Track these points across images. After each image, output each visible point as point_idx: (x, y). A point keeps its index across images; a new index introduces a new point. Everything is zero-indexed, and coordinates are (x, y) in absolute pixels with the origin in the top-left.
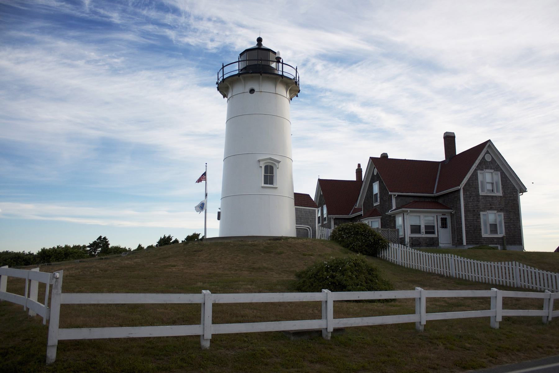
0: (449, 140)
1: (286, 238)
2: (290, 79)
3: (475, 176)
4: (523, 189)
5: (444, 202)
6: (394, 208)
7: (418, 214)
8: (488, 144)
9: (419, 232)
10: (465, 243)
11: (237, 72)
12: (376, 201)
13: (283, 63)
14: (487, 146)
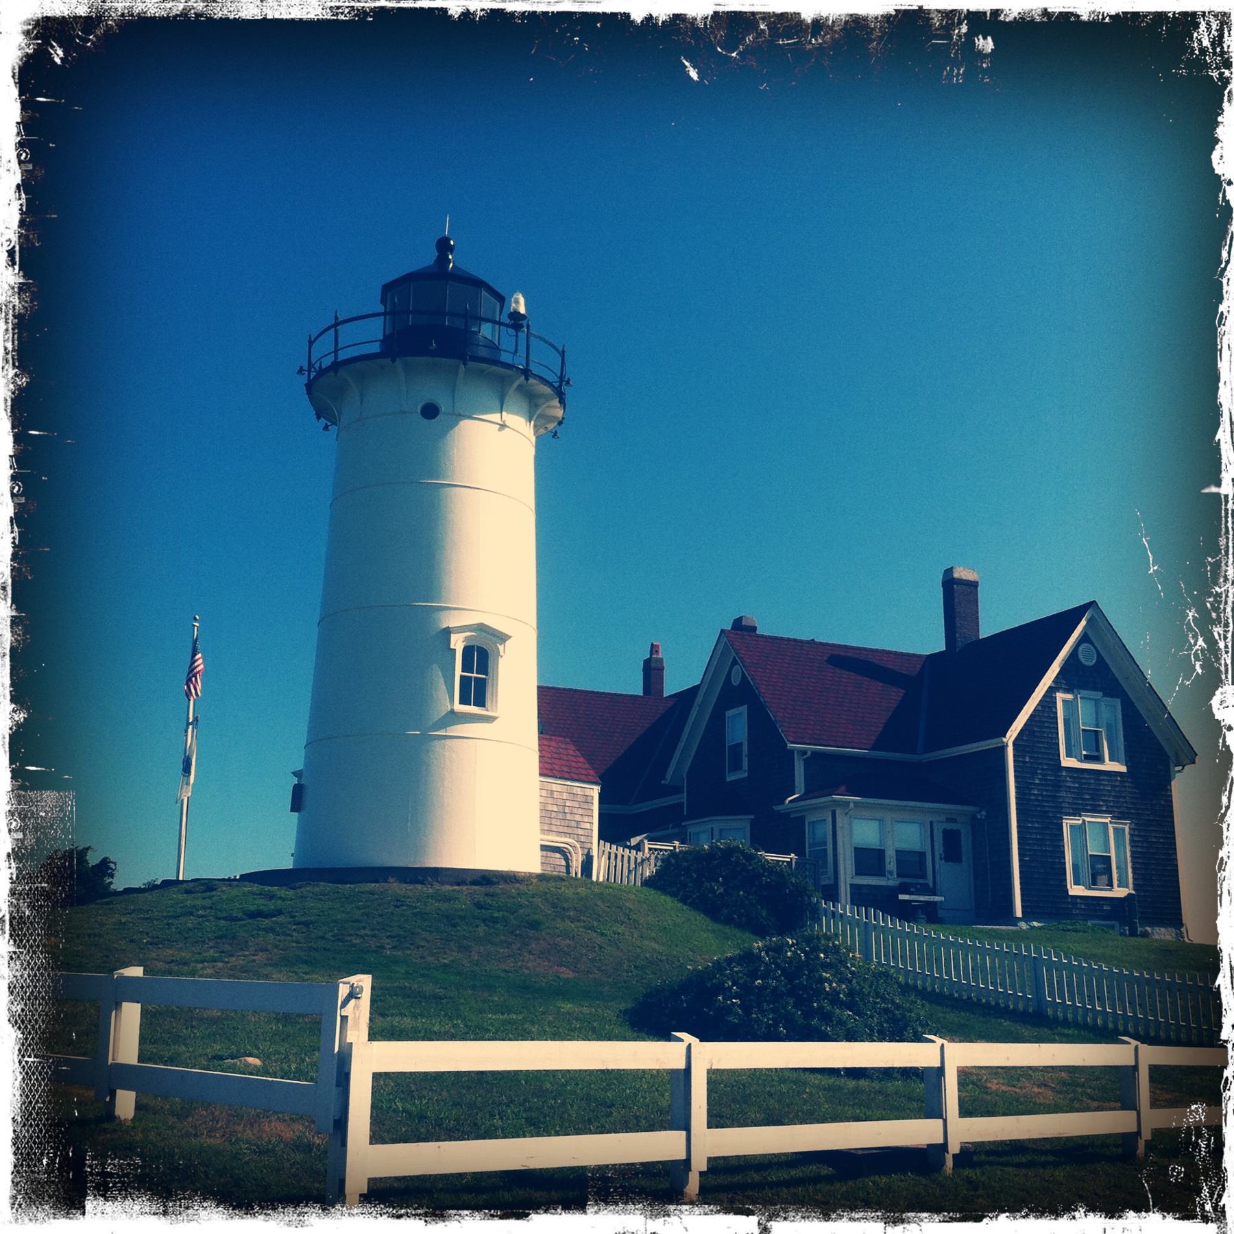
0: (958, 597)
1: (509, 878)
7: (879, 815)
9: (880, 871)
11: (375, 348)
12: (737, 766)
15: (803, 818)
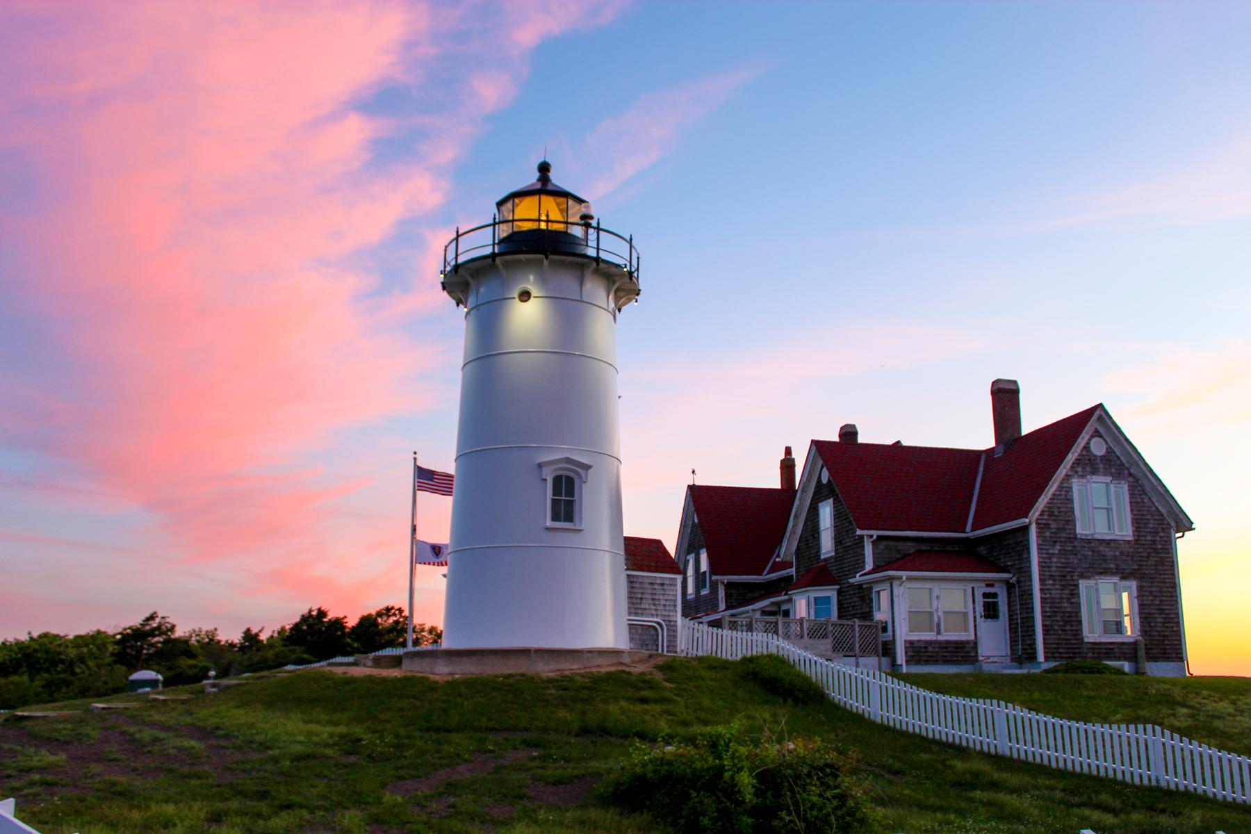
0: (1005, 398)
2: (618, 266)
3: (1065, 498)
4: (1185, 525)
5: (994, 555)
6: (869, 566)
8: (1097, 413)
10: (1041, 656)
11: (488, 251)
13: (598, 229)
14: (1094, 418)
15: (871, 588)
